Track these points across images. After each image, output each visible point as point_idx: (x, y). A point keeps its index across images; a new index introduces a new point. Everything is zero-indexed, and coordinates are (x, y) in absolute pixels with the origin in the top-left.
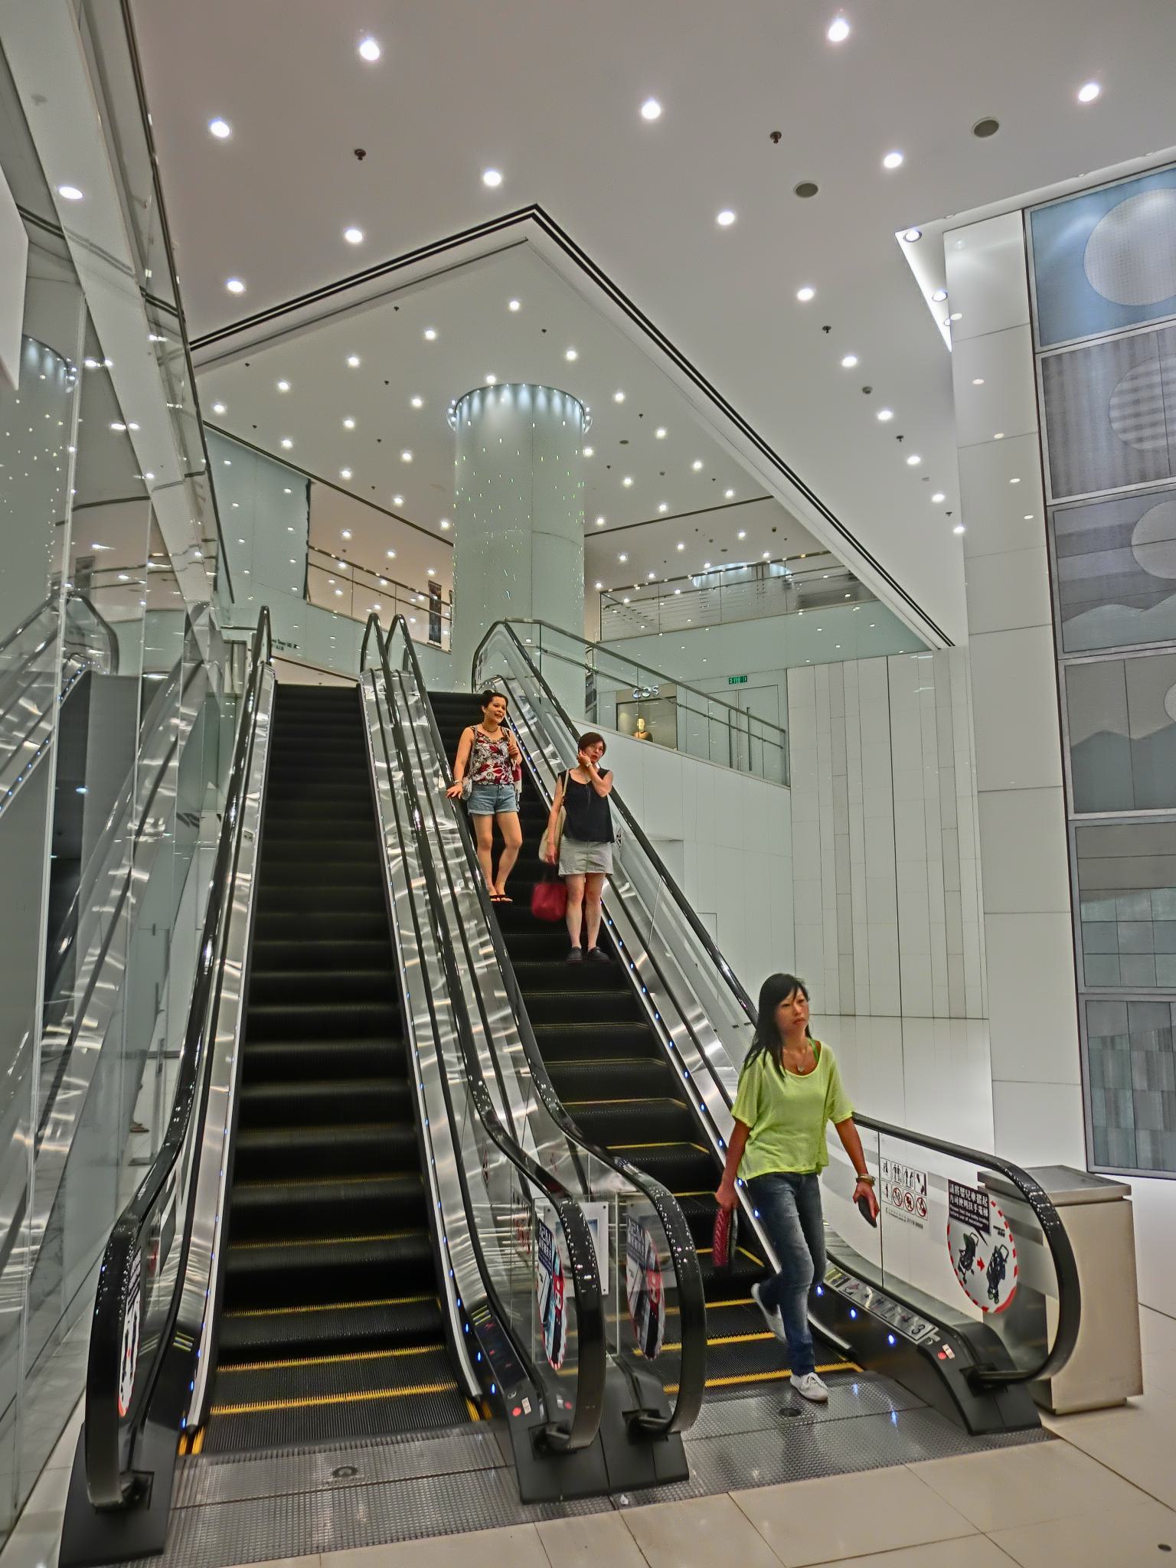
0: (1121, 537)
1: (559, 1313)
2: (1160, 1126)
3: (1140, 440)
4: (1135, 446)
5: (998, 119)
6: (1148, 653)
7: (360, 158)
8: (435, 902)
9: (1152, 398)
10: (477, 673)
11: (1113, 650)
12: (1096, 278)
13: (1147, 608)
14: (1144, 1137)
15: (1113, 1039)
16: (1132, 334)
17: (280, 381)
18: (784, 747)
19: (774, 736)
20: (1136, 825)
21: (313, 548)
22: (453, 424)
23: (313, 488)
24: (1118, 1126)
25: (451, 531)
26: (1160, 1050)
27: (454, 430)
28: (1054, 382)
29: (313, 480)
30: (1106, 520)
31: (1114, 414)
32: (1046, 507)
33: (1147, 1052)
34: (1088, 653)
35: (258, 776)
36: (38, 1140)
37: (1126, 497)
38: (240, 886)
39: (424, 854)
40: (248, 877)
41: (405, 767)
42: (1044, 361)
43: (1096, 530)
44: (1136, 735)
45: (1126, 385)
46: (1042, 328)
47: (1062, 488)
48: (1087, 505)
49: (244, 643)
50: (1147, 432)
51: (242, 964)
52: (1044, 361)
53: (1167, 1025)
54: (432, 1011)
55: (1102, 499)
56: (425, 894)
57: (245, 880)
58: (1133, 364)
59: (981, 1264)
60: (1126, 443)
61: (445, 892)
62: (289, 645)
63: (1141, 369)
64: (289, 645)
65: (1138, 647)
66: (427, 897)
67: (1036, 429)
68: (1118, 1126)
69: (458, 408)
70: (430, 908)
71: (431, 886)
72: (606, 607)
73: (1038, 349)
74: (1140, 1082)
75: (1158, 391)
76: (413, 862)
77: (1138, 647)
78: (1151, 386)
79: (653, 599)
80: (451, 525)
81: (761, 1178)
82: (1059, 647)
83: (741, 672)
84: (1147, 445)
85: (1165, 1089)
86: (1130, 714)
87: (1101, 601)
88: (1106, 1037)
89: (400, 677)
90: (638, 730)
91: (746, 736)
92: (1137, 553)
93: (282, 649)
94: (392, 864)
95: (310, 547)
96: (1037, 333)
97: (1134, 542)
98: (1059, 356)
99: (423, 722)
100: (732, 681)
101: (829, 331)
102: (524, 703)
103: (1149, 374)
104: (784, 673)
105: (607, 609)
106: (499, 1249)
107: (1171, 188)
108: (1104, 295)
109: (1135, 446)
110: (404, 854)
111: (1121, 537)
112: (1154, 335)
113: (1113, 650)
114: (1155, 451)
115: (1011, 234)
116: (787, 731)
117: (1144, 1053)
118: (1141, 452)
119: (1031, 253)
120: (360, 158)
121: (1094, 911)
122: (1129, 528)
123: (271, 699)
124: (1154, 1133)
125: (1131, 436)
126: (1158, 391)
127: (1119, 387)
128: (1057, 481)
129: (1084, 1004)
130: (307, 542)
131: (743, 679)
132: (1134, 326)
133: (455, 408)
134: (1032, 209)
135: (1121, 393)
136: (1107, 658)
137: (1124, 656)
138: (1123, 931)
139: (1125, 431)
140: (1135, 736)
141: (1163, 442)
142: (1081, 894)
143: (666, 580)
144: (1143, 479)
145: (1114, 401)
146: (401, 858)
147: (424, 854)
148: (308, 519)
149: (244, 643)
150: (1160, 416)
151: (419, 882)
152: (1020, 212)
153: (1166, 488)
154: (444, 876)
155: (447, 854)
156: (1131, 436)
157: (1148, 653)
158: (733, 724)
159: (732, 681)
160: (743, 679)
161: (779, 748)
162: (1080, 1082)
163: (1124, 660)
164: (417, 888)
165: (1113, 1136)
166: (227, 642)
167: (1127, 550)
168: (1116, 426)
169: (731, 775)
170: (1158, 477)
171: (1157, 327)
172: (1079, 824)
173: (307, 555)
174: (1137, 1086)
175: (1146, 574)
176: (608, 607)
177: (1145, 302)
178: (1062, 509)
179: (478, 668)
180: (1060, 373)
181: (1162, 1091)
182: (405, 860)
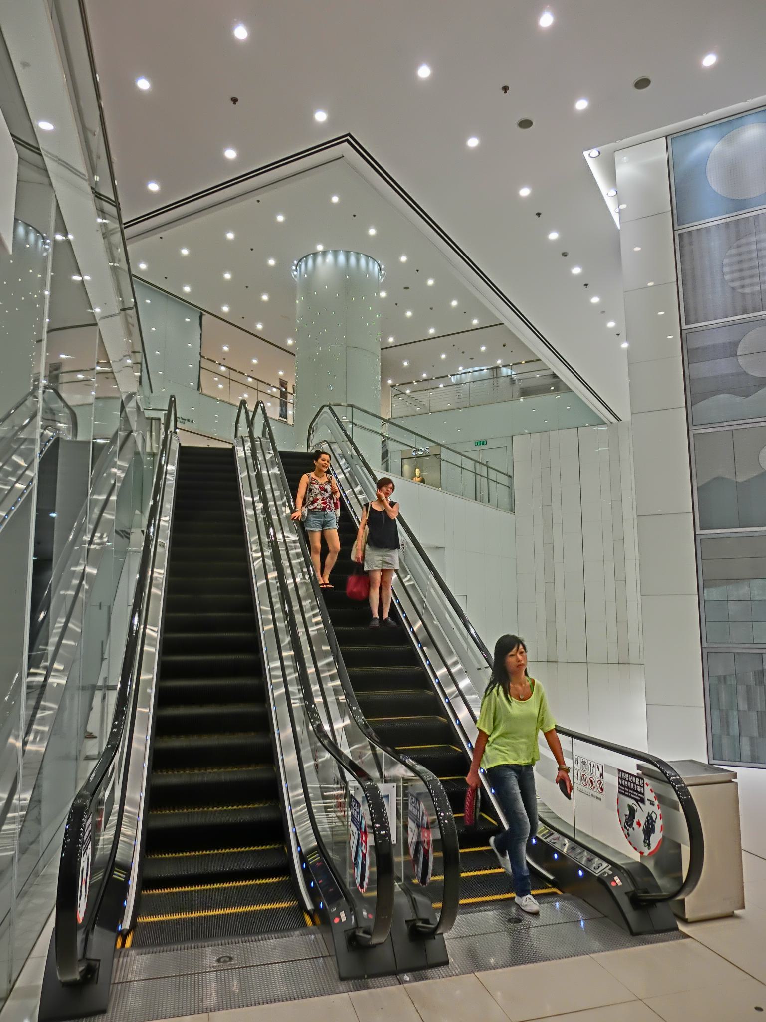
0: (730, 350)
1: (364, 856)
2: (756, 734)
3: (743, 287)
4: (740, 291)
5: (650, 78)
6: (748, 426)
7: (235, 103)
8: (283, 588)
9: (751, 260)
10: (311, 439)
11: (725, 424)
12: (714, 181)
13: (747, 396)
14: (745, 741)
15: (725, 677)
16: (737, 217)
17: (183, 248)
18: (510, 487)
19: (504, 480)
20: (740, 538)
21: (204, 357)
22: (295, 276)
23: (204, 318)
24: (728, 734)
25: (294, 346)
26: (756, 685)
27: (296, 280)
28: (687, 249)
29: (204, 313)
30: (721, 339)
31: (726, 270)
32: (681, 330)
33: (747, 686)
34: (708, 426)
35: (168, 506)
37: (734, 324)
38: (156, 577)
39: (276, 557)
40: (162, 571)
41: (264, 500)
42: (680, 235)
43: (714, 346)
44: (740, 479)
45: (733, 251)
46: (679, 214)
47: (692, 318)
48: (708, 329)
49: (159, 419)
50: (747, 282)
51: (158, 629)
52: (680, 235)
53: (760, 668)
54: (281, 659)
55: (718, 325)
56: (277, 583)
57: (160, 574)
58: (738, 238)
59: (639, 824)
60: (733, 289)
61: (290, 581)
62: (188, 421)
63: (743, 241)
64: (188, 421)
65: (741, 422)
66: (278, 585)
67: (675, 280)
68: (728, 734)
69: (298, 266)
70: (280, 591)
71: (281, 577)
72: (395, 396)
73: (676, 227)
74: (742, 705)
75: (754, 255)
76: (269, 562)
77: (741, 422)
78: (749, 252)
79: (425, 390)
80: (294, 342)
81: (496, 768)
82: (690, 422)
83: (483, 438)
84: (747, 290)
85: (759, 710)
86: (736, 466)
87: (717, 392)
88: (720, 676)
89: (260, 441)
90: (416, 476)
91: (486, 480)
92: (741, 360)
93: (184, 423)
94: (256, 563)
95: (202, 357)
96: (675, 217)
97: (738, 353)
98: (690, 232)
99: (276, 470)
100: (477, 444)
101: (540, 216)
103: (748, 244)
104: (510, 439)
105: (395, 397)
106: (325, 814)
107: (763, 123)
108: (719, 192)
109: (740, 291)
110: (263, 557)
111: (730, 350)
112: (752, 218)
113: (725, 424)
114: (753, 294)
115: (659, 153)
116: (512, 476)
117: (745, 686)
118: (743, 295)
119: (671, 165)
120: (235, 103)
121: (713, 594)
122: (736, 344)
123: (177, 456)
124: (751, 739)
125: (737, 284)
126: (754, 255)
127: (729, 253)
128: (688, 313)
129: (706, 655)
130: (200, 354)
131: (484, 443)
132: (738, 212)
133: (297, 266)
134: (672, 136)
135: (730, 256)
136: (721, 429)
137: (732, 428)
138: (732, 606)
139: (733, 281)
140: (739, 480)
141: (757, 288)
142: (704, 583)
143: (434, 378)
144: (745, 312)
145: (726, 261)
146: (261, 559)
147: (276, 557)
148: (201, 338)
149: (159, 419)
150: (756, 271)
151: (273, 575)
152: (665, 138)
153: (760, 318)
154: (289, 571)
155: (291, 556)
156: (737, 284)
157: (748, 426)
158: (478, 472)
159: (477, 444)
160: (484, 443)
161: (507, 488)
162: (703, 705)
163: (732, 430)
164: (272, 579)
165: (725, 741)
166: (148, 418)
167: (734, 358)
168: (727, 277)
169: (476, 505)
170: (754, 311)
171: (753, 213)
172: (703, 537)
173: (200, 362)
174: (741, 708)
175: (747, 374)
176: (396, 395)
177: (746, 197)
178: (692, 332)
179: (311, 436)
180: (691, 243)
181: (757, 711)
182: (264, 561)
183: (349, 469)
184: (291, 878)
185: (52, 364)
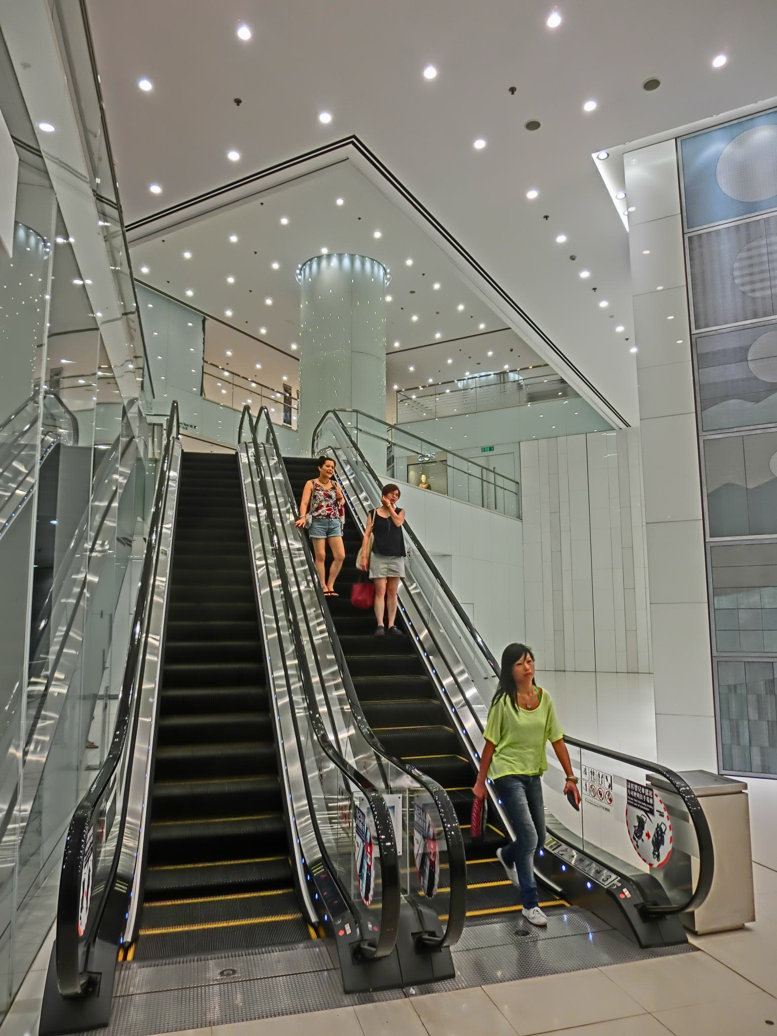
0: (741, 355)
1: (369, 867)
2: (766, 744)
3: (753, 291)
4: (750, 295)
5: (660, 79)
6: (758, 432)
7: (238, 105)
8: (287, 596)
9: (761, 263)
10: (315, 445)
11: (736, 429)
12: (724, 184)
13: (758, 402)
14: (756, 751)
15: (735, 686)
16: (748, 220)
17: (185, 252)
18: (518, 494)
19: (512, 486)
20: (751, 545)
21: (207, 362)
22: (299, 280)
23: (207, 322)
24: (739, 744)
25: (298, 351)
26: (766, 694)
27: (300, 284)
28: (696, 252)
29: (207, 317)
30: (731, 343)
31: (736, 273)
32: (691, 335)
33: (758, 695)
34: (719, 432)
35: (171, 513)
36: (25, 753)
37: (744, 328)
38: (159, 585)
39: (280, 564)
40: (164, 579)
41: (268, 507)
42: (690, 238)
43: (724, 350)
44: (751, 486)
45: (744, 255)
46: (689, 217)
47: (702, 322)
48: (718, 334)
49: (161, 425)
50: (758, 286)
51: (160, 637)
52: (690, 238)
53: (771, 677)
54: (285, 668)
55: (728, 330)
56: (281, 590)
57: (162, 581)
58: (749, 241)
59: (648, 835)
60: (744, 293)
61: (294, 589)
62: (191, 426)
63: (754, 244)
64: (191, 426)
65: (752, 428)
66: (282, 593)
67: (685, 283)
68: (739, 744)
69: (303, 270)
70: (284, 600)
71: (285, 585)
72: (401, 401)
73: (686, 230)
74: (753, 715)
75: (765, 258)
76: (273, 570)
77: (752, 428)
78: (760, 255)
79: (432, 396)
80: (298, 347)
81: (503, 778)
82: (700, 427)
83: (489, 444)
84: (758, 294)
85: (770, 719)
86: (747, 472)
87: (727, 397)
88: (731, 685)
89: (264, 447)
90: (422, 482)
91: (493, 486)
92: (751, 365)
93: (187, 429)
94: (259, 571)
95: (205, 361)
96: (685, 220)
97: (749, 358)
98: (700, 235)
99: (280, 477)
100: (484, 450)
101: (548, 219)
102: (346, 465)
103: (759, 247)
104: (518, 445)
105: (401, 402)
106: (329, 825)
107: (774, 124)
108: (729, 195)
109: (750, 295)
110: (267, 564)
111: (741, 355)
112: (763, 221)
113: (736, 429)
114: (763, 298)
115: (668, 155)
116: (520, 483)
117: (756, 696)
118: (754, 299)
119: (681, 167)
120: (238, 105)
121: (723, 602)
122: (746, 349)
123: (179, 462)
124: (762, 749)
125: (747, 288)
126: (765, 258)
127: (739, 256)
128: (698, 318)
129: (717, 664)
130: (203, 358)
131: (491, 449)
132: (749, 215)
133: (301, 270)
134: (682, 138)
135: (741, 259)
136: (731, 435)
137: (743, 433)
138: (742, 615)
139: (743, 285)
140: (750, 486)
141: (768, 292)
142: (714, 591)
143: (440, 383)
144: (755, 316)
145: (736, 265)
146: (265, 567)
147: (280, 564)
148: (204, 343)
149: (161, 425)
150: (767, 275)
151: (277, 583)
152: (674, 140)
153: (771, 322)
154: (293, 579)
155: (295, 564)
156: (747, 288)
157: (758, 432)
158: (484, 478)
159: (484, 450)
160: (491, 449)
161: (515, 494)
162: (713, 715)
163: (743, 436)
164: (276, 587)
165: (735, 751)
166: (150, 424)
167: (744, 363)
168: (737, 281)
169: (483, 512)
170: (765, 315)
171: (764, 216)
172: (713, 544)
173: (203, 367)
174: (751, 718)
175: (757, 379)
176: (401, 401)
177: (756, 200)
178: (702, 336)
179: (316, 442)
180: (701, 246)
181: (768, 721)
182: (267, 569)
183: (354, 475)
184: (296, 890)
185: (53, 369)
